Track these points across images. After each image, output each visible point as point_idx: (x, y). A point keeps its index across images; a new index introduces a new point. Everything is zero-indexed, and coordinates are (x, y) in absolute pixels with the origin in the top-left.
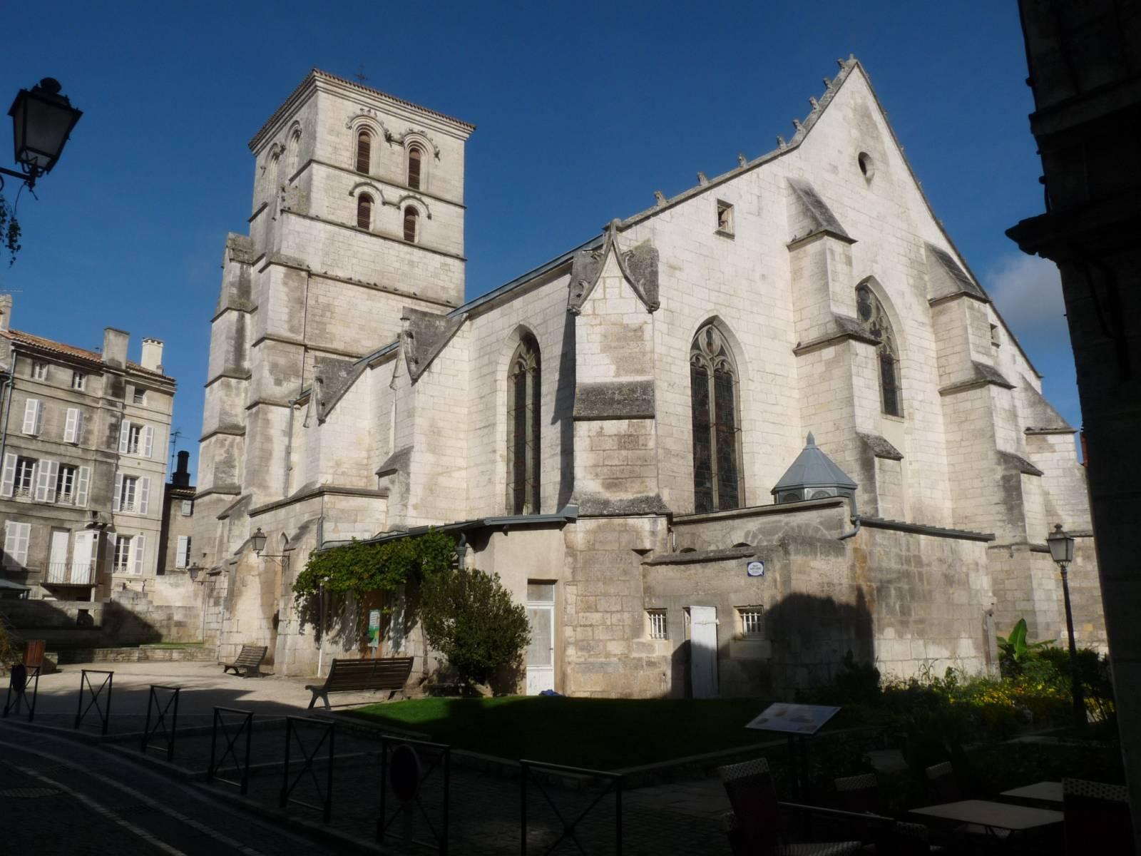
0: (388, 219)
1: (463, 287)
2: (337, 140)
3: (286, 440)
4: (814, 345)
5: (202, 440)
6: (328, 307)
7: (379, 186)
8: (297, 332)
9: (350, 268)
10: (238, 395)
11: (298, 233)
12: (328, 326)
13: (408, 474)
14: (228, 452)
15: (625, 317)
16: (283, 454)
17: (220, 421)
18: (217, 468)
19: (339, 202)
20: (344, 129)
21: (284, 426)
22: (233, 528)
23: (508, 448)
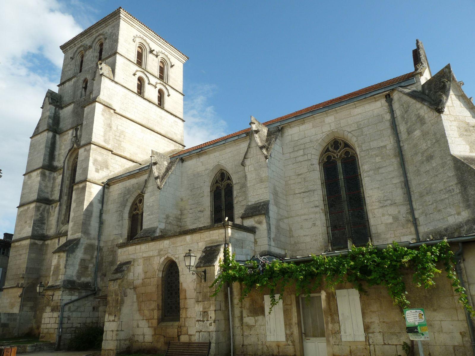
0: (151, 93)
3: (100, 205)
4: (404, 168)
8: (108, 143)
10: (49, 181)
12: (122, 143)
13: (269, 217)
14: (41, 214)
15: (466, 118)
17: (38, 195)
18: (34, 224)
22: (69, 259)
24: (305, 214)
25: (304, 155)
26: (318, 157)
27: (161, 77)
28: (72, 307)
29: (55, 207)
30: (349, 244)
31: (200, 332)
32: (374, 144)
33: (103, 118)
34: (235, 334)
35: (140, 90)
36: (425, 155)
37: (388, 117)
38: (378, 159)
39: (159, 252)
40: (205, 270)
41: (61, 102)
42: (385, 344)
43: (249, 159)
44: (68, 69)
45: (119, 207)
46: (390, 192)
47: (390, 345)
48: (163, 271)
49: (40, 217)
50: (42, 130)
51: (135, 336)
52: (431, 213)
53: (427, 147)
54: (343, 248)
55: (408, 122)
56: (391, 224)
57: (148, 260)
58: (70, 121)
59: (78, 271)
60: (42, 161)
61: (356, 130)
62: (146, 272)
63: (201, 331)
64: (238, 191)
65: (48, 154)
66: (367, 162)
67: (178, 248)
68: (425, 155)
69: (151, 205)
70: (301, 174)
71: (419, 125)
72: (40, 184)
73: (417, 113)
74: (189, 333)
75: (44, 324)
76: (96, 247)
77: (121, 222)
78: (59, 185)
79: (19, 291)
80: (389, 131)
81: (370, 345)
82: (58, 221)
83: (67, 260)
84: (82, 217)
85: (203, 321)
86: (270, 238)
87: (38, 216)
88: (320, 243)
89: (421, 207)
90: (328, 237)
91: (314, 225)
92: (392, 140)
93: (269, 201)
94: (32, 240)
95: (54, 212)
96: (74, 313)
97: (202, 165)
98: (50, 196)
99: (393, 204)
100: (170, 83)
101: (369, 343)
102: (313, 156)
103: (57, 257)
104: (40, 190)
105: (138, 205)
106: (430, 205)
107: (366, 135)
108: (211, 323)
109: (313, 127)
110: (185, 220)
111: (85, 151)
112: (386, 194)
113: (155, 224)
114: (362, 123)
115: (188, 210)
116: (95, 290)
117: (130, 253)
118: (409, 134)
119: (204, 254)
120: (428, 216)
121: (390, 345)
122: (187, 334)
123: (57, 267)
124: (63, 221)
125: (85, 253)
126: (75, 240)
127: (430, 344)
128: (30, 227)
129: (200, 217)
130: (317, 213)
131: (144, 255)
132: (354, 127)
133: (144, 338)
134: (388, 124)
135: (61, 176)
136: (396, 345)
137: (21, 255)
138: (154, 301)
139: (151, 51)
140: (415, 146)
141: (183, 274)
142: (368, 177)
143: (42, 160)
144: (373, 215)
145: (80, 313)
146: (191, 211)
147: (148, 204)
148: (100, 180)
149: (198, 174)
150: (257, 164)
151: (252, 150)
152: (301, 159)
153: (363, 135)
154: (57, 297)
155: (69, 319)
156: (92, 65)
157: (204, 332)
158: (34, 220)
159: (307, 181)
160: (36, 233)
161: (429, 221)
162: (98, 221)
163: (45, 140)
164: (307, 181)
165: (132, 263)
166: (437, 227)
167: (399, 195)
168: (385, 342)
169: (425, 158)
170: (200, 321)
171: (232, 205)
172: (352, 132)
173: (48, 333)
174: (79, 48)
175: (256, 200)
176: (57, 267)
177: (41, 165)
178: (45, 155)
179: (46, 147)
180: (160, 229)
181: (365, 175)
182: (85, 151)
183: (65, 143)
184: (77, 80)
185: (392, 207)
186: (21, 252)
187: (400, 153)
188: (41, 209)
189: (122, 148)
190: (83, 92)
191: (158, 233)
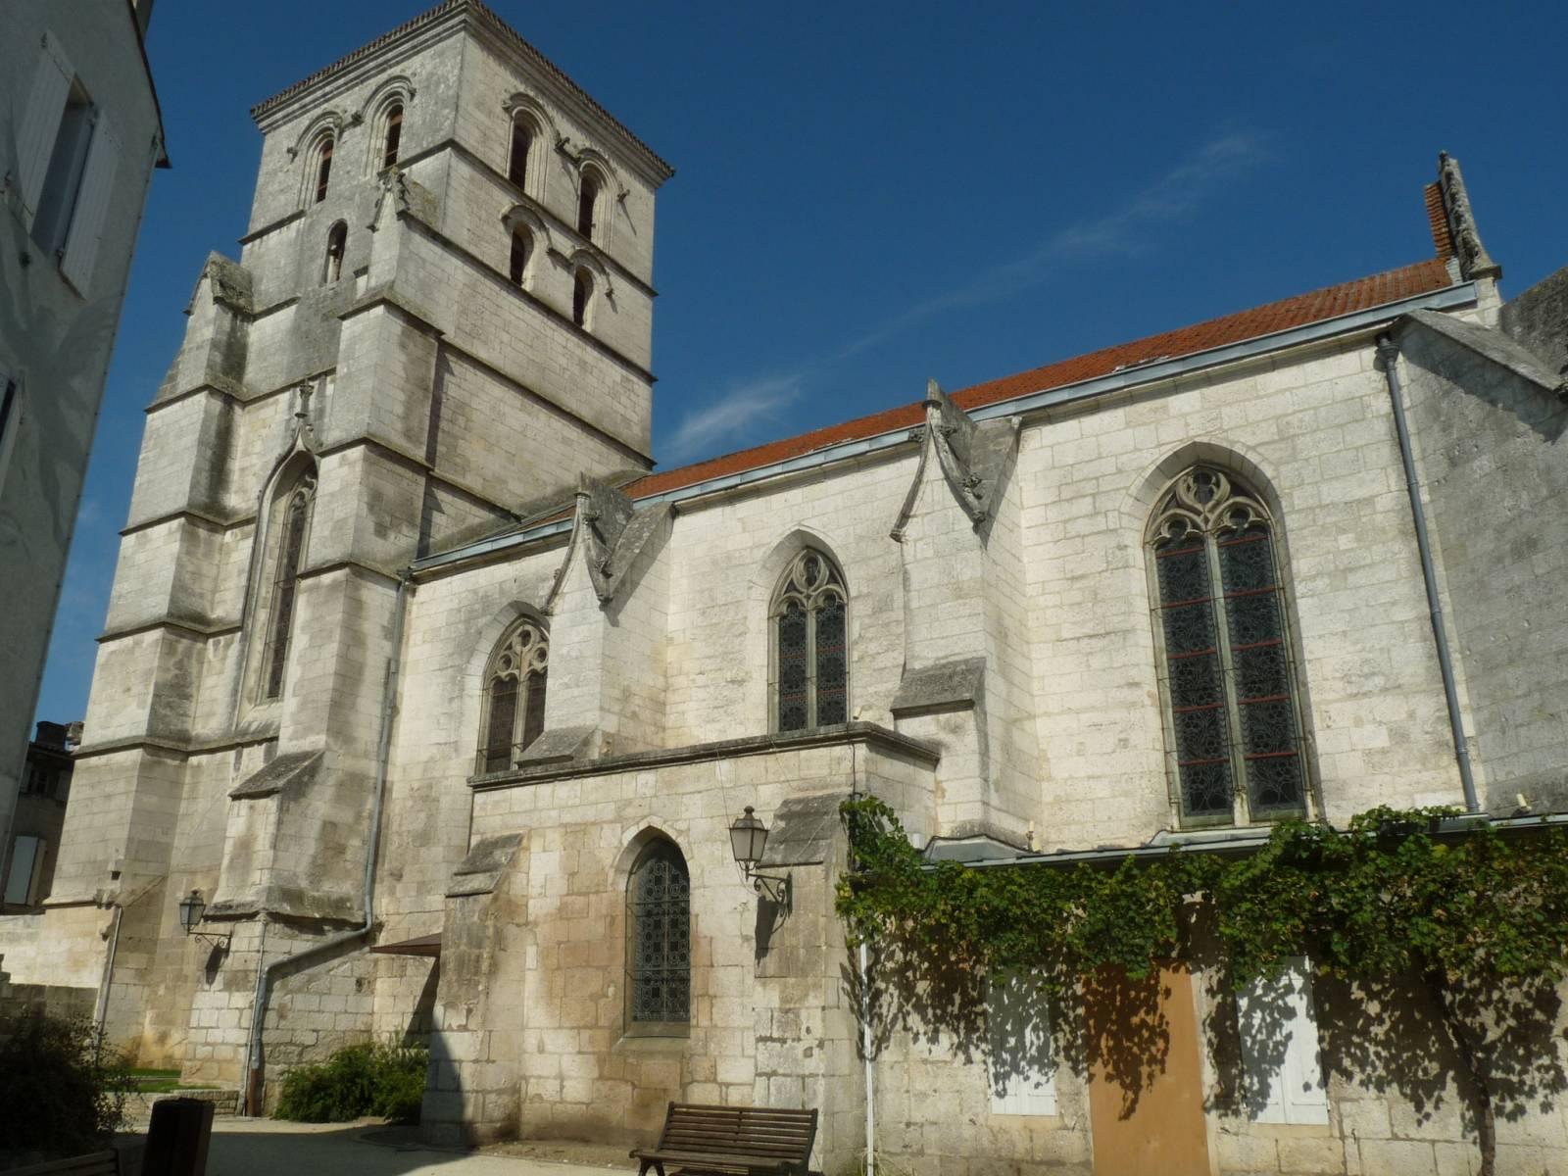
1: (648, 422)
2: (487, 122)
5: (102, 640)
9: (497, 348)
11: (424, 261)
12: (461, 441)
13: (985, 714)
16: (382, 673)
17: (173, 601)
18: (156, 695)
19: (486, 227)
21: (385, 619)
22: (287, 818)
23: (1158, 680)
24: (1093, 708)
25: (1096, 513)
26: (1141, 525)
29: (228, 646)
30: (1241, 811)
31: (769, 1075)
32: (1333, 492)
34: (881, 1087)
36: (1510, 534)
37: (1383, 404)
38: (1345, 541)
39: (619, 810)
40: (790, 876)
41: (251, 296)
42: (1395, 1137)
43: (919, 519)
44: (276, 186)
45: (451, 655)
46: (1382, 649)
47: (1412, 1140)
48: (631, 873)
49: (176, 676)
50: (189, 388)
51: (532, 1080)
52: (1521, 725)
54: (1220, 824)
55: (1451, 426)
56: (1384, 751)
58: (284, 359)
59: (315, 858)
60: (187, 488)
63: (774, 1073)
64: (867, 621)
65: (207, 466)
66: (1308, 547)
67: (685, 799)
68: (1510, 534)
69: (574, 654)
70: (1082, 577)
72: (180, 565)
74: (721, 1078)
75: (198, 1028)
76: (372, 781)
77: (455, 704)
78: (240, 572)
79: (104, 919)
81: (1343, 1137)
82: (235, 692)
83: (280, 823)
84: (330, 683)
85: (783, 1041)
86: (986, 780)
87: (168, 670)
88: (1141, 801)
90: (1169, 784)
91: (1124, 743)
93: (983, 660)
95: (224, 659)
96: (299, 997)
97: (744, 530)
98: (208, 608)
99: (1393, 688)
101: (1341, 1131)
102: (1125, 519)
103: (244, 811)
104: (179, 588)
105: (518, 648)
106: (1518, 697)
107: (1307, 460)
108: (811, 1048)
109: (1128, 425)
110: (681, 707)
111: (341, 465)
113: (589, 715)
114: (1294, 420)
115: (692, 677)
116: (364, 925)
117: (516, 809)
118: (1453, 463)
120: (1511, 733)
121: (1412, 1140)
122: (715, 1081)
123: (245, 845)
124: (251, 692)
125: (338, 799)
126: (305, 756)
127: (1548, 1142)
128: (141, 705)
129: (730, 702)
130: (1133, 704)
131: (567, 818)
132: (1267, 432)
133: (562, 1087)
134: (1382, 429)
135: (250, 541)
136: (1433, 1142)
137: (108, 797)
138: (598, 968)
140: (1477, 504)
142: (1312, 596)
143: (187, 487)
144: (1323, 720)
145: (316, 999)
146: (701, 680)
147: (564, 650)
148: (392, 562)
149: (729, 558)
151: (928, 490)
152: (1083, 527)
153: (1295, 460)
154: (246, 941)
155: (282, 1017)
156: (363, 179)
157: (784, 1075)
158: (156, 685)
159: (1103, 601)
160: (161, 727)
161: (1515, 749)
162: (380, 698)
163: (198, 417)
164: (1103, 601)
165: (525, 842)
166: (1542, 770)
168: (1396, 1130)
169: (1508, 547)
170: (771, 1039)
172: (1261, 450)
173: (211, 1059)
175: (941, 654)
176: (245, 845)
177: (181, 502)
178: (197, 470)
179: (201, 443)
180: (604, 733)
182: (341, 465)
183: (902, 448)
184: (311, 227)
185: (1389, 699)
186: (109, 789)
189: (458, 460)
190: (331, 268)
191: (595, 754)
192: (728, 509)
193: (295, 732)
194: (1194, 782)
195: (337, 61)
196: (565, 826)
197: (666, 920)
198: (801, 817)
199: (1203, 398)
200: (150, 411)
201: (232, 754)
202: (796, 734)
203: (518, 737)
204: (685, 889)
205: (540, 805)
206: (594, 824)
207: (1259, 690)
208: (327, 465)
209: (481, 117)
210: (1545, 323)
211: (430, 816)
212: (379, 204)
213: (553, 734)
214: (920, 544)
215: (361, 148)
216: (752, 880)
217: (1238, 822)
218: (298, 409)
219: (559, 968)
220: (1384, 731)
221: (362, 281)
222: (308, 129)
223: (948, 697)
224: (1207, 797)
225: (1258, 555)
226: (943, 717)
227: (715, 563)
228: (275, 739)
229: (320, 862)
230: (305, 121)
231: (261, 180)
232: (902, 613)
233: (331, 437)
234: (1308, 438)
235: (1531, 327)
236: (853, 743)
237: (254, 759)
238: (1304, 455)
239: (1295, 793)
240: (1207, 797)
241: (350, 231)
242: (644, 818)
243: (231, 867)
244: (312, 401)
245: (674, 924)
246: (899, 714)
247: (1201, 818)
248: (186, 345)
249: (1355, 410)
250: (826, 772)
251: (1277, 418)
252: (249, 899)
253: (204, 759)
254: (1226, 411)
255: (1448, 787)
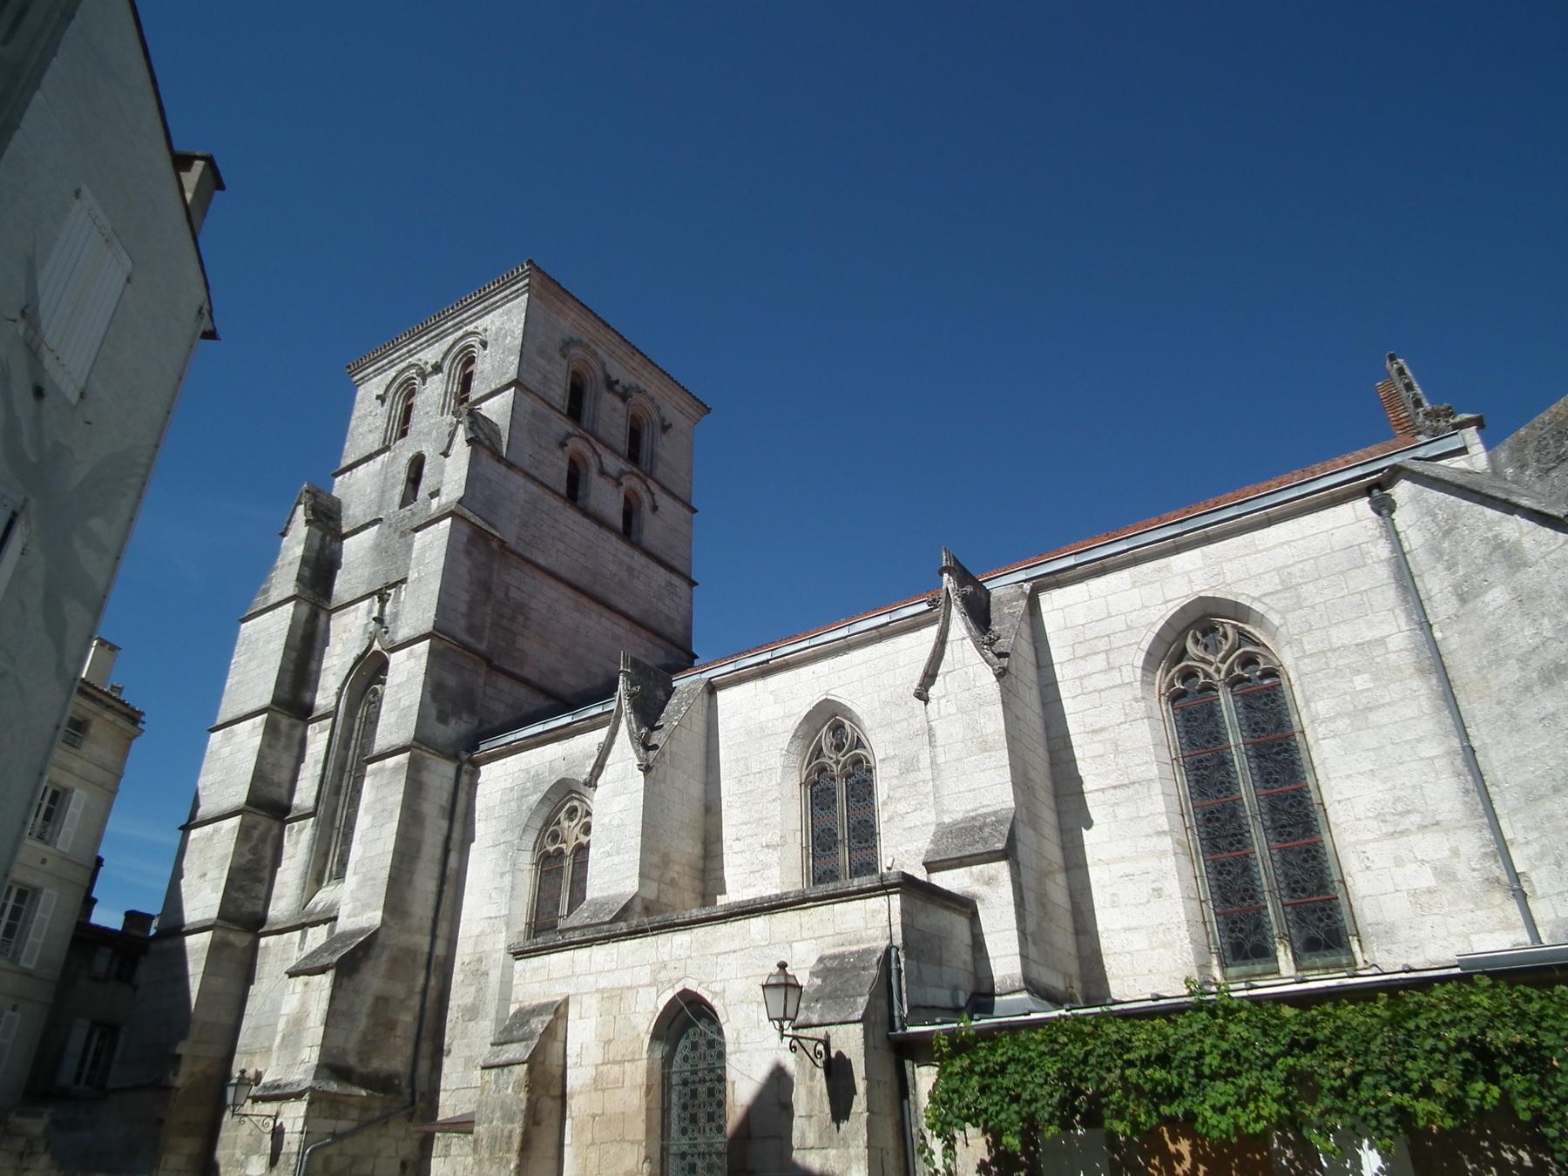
3: (444, 824)
6: (521, 608)
7: (599, 447)
8: (480, 639)
20: (557, 356)
24: (1123, 859)
27: (633, 456)
28: (335, 1159)
29: (300, 831)
30: (1285, 960)
32: (1342, 635)
33: (467, 563)
35: (573, 491)
36: (1536, 662)
37: (1383, 550)
38: (1361, 682)
46: (1414, 787)
53: (1538, 640)
56: (1430, 891)
57: (616, 1000)
59: (364, 1034)
61: (1277, 592)
62: (609, 1041)
64: (895, 782)
65: (292, 667)
69: (615, 823)
70: (1102, 730)
71: (1499, 571)
73: (1490, 535)
78: (316, 762)
80: (1391, 594)
89: (1533, 835)
91: (1158, 892)
92: (1402, 620)
94: (219, 933)
95: (297, 843)
100: (661, 472)
103: (299, 988)
112: (1401, 793)
114: (1295, 570)
117: (555, 975)
118: (1463, 600)
119: (818, 981)
130: (1164, 853)
131: (603, 983)
132: (1271, 583)
134: (1384, 573)
138: (632, 1143)
139: (611, 384)
140: (1495, 636)
141: (741, 1051)
143: (272, 687)
147: (606, 820)
150: (967, 694)
152: (1100, 681)
159: (1125, 751)
164: (1125, 751)
167: (1446, 793)
169: (1535, 675)
171: (873, 826)
172: (1266, 600)
174: (404, 370)
176: (298, 1022)
181: (1321, 730)
185: (1428, 836)
187: (1436, 663)
188: (256, 834)
192: (760, 683)
193: (355, 908)
194: (1232, 931)
195: (419, 319)
196: (602, 991)
197: (702, 1089)
198: (835, 970)
199: (1204, 556)
200: (244, 620)
201: (298, 933)
202: (830, 887)
203: (563, 910)
204: (721, 1055)
205: (578, 970)
206: (629, 988)
207: (1290, 834)
208: (396, 659)
209: (542, 362)
210: (1538, 461)
211: (479, 990)
212: (452, 435)
213: (594, 902)
214: (943, 701)
215: (433, 392)
216: (787, 1040)
217: (1284, 973)
218: (375, 614)
219: (593, 1143)
220: (1427, 869)
221: (435, 502)
222: (395, 379)
223: (979, 848)
224: (1248, 946)
225: (1274, 701)
226: (976, 869)
227: (749, 733)
228: (335, 919)
229: (370, 1038)
230: (392, 373)
231: (353, 423)
232: (929, 772)
233: (402, 634)
234: (1311, 587)
235: (1523, 467)
236: (888, 894)
237: (318, 936)
238: (1308, 603)
239: (1340, 939)
240: (1248, 946)
241: (427, 461)
242: (679, 980)
243: (283, 1045)
244: (388, 607)
245: (711, 1092)
246: (931, 867)
247: (1244, 968)
248: (279, 563)
249: (1356, 557)
250: (861, 924)
251: (1278, 569)
252: (297, 1077)
253: (272, 939)
254: (1227, 566)
255: (1508, 926)
